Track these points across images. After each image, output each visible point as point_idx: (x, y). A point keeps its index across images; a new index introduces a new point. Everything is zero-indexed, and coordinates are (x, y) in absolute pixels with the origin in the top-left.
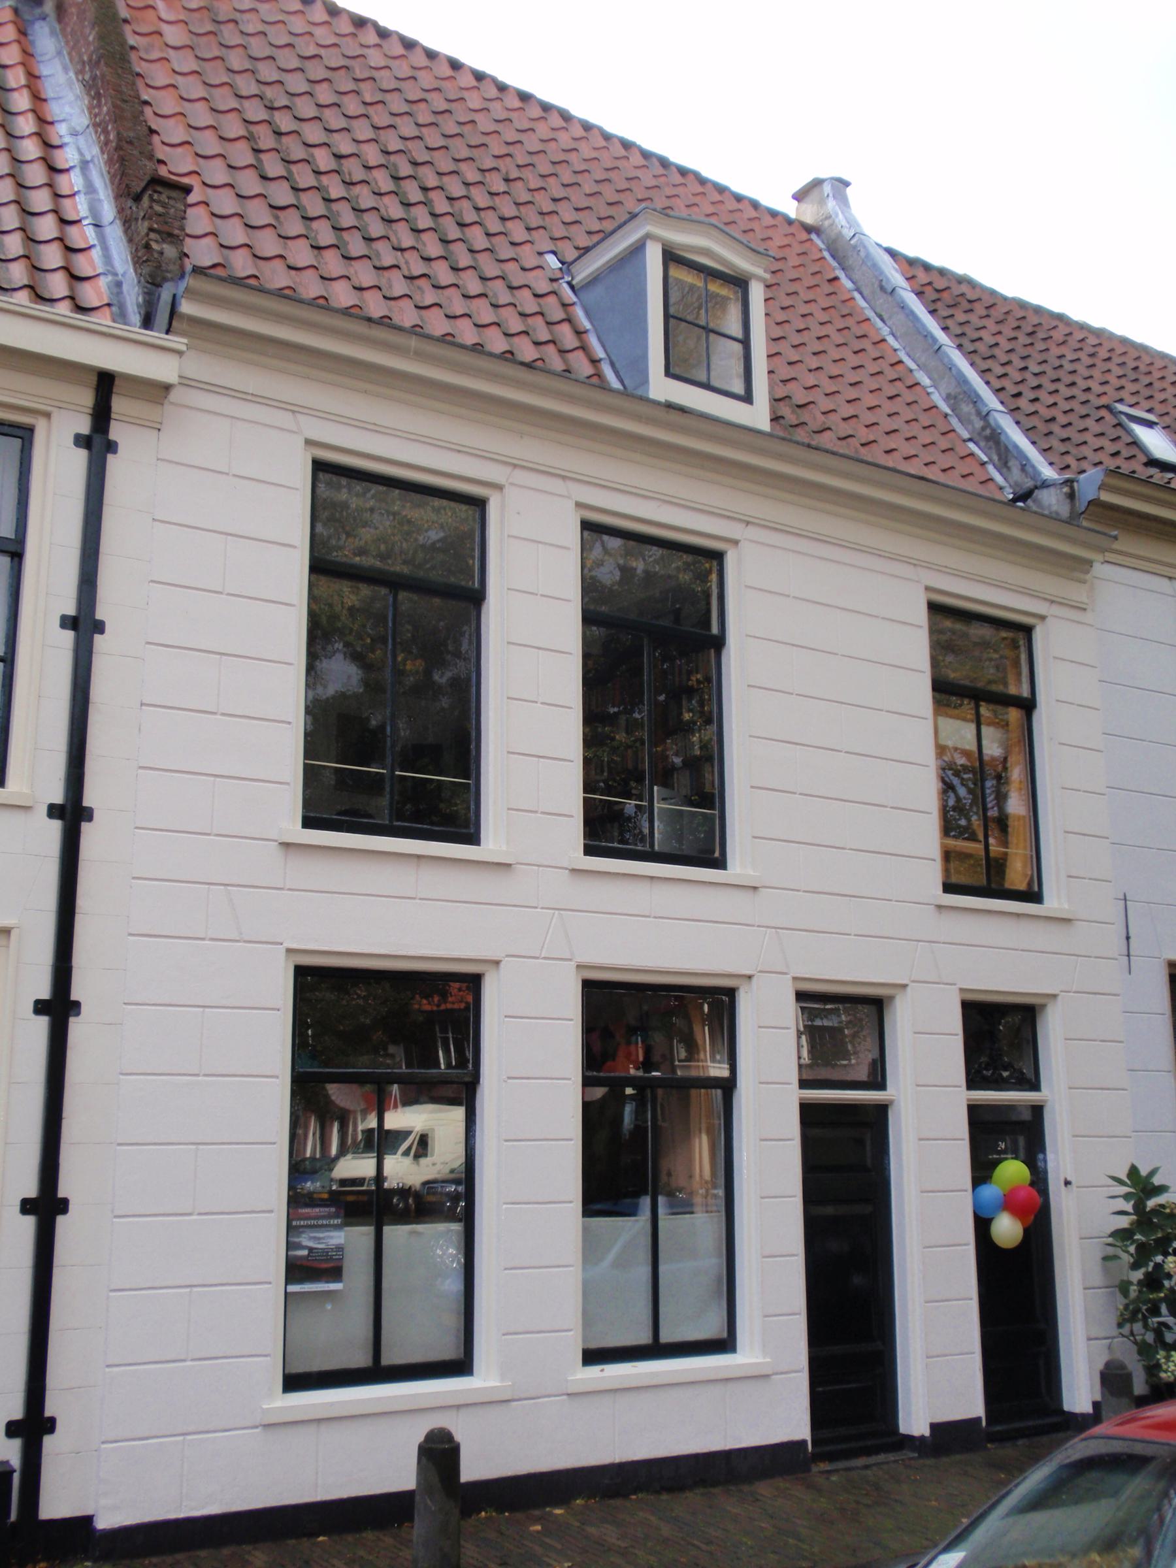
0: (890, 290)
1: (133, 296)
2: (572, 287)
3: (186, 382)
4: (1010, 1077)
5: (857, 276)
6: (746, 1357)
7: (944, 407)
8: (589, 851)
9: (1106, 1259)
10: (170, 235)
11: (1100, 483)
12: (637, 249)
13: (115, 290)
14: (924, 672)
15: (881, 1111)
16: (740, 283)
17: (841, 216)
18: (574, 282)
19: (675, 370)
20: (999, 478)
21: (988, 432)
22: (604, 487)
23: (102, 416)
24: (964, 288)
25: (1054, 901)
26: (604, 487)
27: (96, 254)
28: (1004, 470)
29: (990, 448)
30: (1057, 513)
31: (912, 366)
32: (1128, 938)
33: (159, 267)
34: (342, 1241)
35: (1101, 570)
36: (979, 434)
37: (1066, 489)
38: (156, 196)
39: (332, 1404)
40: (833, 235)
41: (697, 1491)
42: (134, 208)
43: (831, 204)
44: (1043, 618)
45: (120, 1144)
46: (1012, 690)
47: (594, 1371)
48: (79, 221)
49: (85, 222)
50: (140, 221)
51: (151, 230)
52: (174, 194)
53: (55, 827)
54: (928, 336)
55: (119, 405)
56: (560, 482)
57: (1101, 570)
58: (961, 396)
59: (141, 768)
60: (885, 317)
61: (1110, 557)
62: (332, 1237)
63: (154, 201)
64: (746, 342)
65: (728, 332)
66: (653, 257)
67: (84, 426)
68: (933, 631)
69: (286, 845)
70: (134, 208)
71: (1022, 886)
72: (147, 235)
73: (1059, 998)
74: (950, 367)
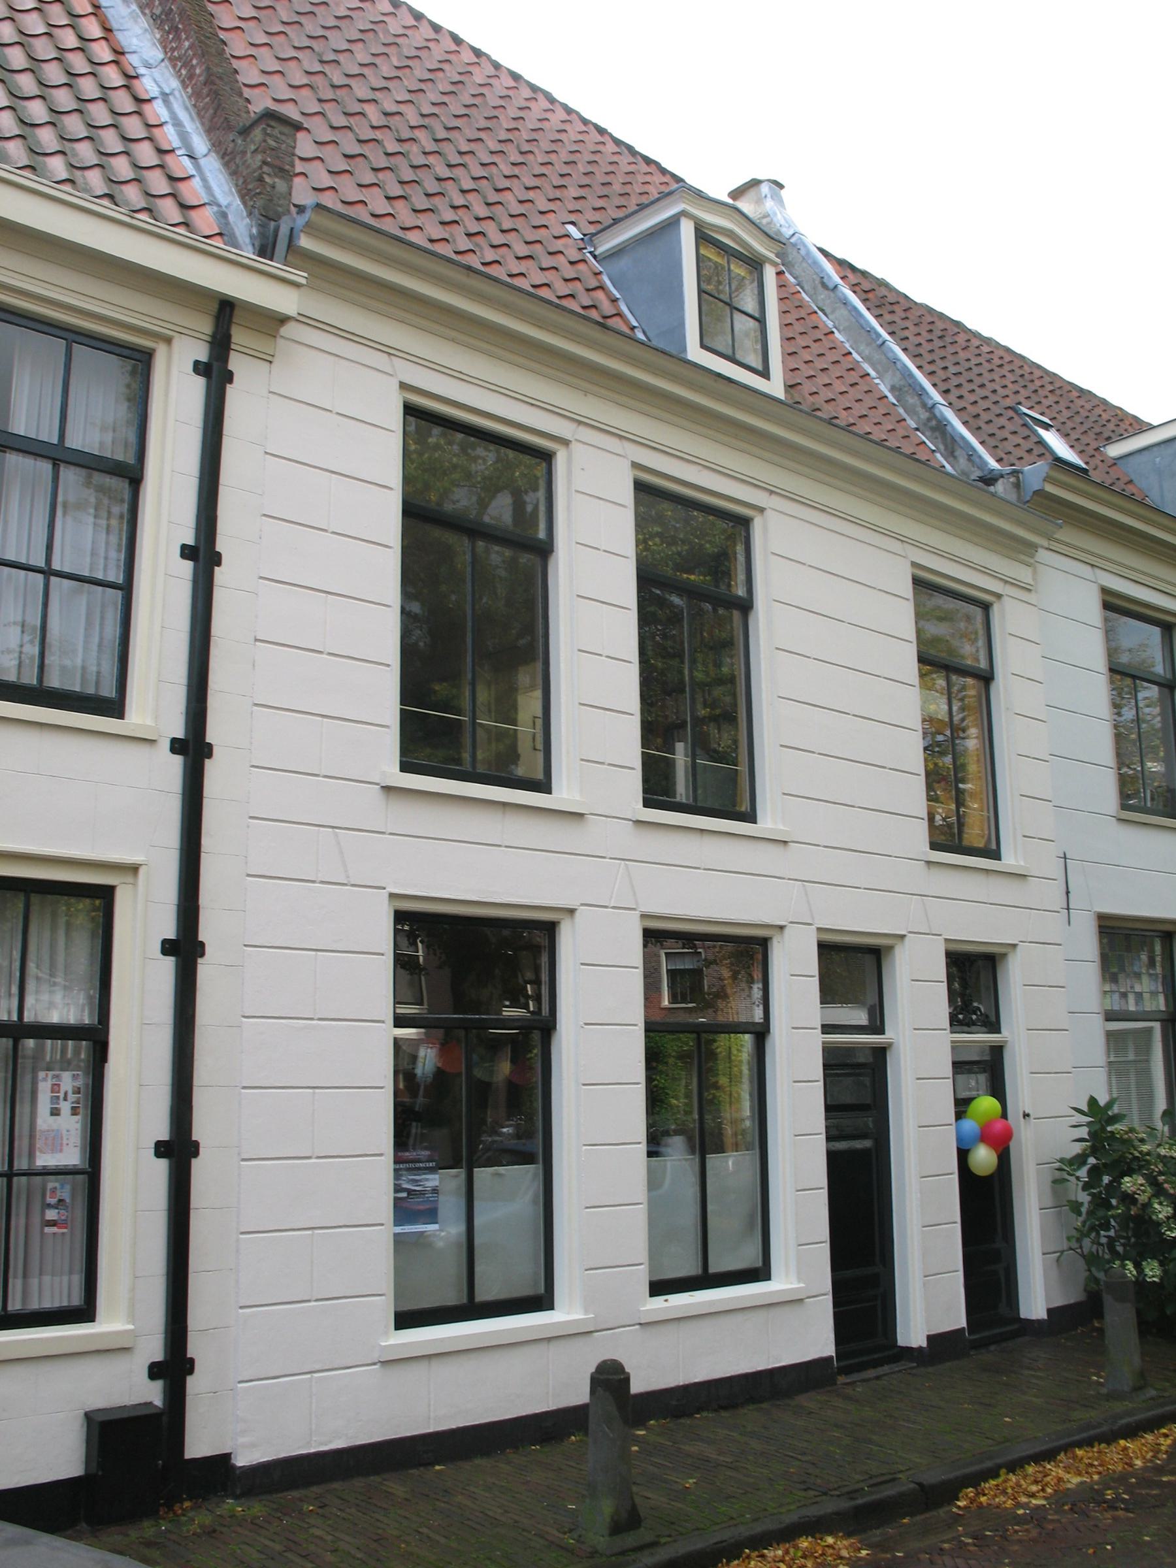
1: (243, 226)
2: (595, 257)
3: (303, 320)
4: (978, 1019)
6: (780, 1283)
7: (892, 399)
8: (647, 804)
9: (1055, 1182)
10: (282, 170)
11: (1045, 475)
12: (669, 225)
13: (223, 221)
14: (911, 642)
15: (881, 1053)
16: (755, 264)
17: (779, 216)
18: (597, 253)
19: (707, 342)
21: (934, 423)
22: (654, 448)
23: (221, 345)
24: (883, 291)
25: (1010, 859)
26: (654, 448)
27: (196, 182)
28: (951, 459)
29: (936, 438)
31: (859, 358)
32: (1068, 893)
33: (271, 200)
34: (437, 1183)
36: (925, 425)
37: (1012, 479)
38: (269, 130)
39: (442, 1340)
41: (751, 1408)
42: (239, 141)
45: (244, 1088)
47: (659, 1302)
48: (173, 151)
49: (179, 152)
50: (249, 155)
51: (265, 163)
52: (286, 130)
53: (176, 764)
54: (871, 331)
55: (239, 336)
56: (615, 441)
57: (1043, 555)
58: (906, 389)
59: (256, 705)
60: (828, 311)
61: (1055, 546)
62: (427, 1180)
63: (268, 135)
64: (761, 320)
65: (745, 309)
66: (687, 231)
67: (201, 353)
69: (388, 789)
70: (239, 141)
71: (980, 844)
72: (261, 168)
74: (895, 361)
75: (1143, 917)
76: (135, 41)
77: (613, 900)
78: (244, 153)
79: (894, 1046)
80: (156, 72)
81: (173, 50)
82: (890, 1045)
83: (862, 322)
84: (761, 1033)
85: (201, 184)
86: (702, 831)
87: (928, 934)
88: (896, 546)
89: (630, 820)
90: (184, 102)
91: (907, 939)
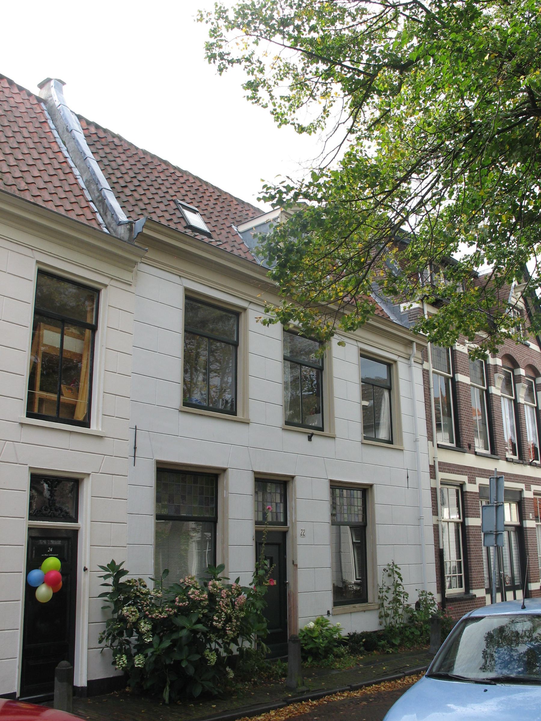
0: (70, 131)
5: (58, 123)
7: (83, 185)
20: (100, 220)
24: (116, 141)
25: (95, 427)
28: (104, 217)
30: (123, 238)
32: (135, 448)
35: (142, 267)
36: (97, 199)
40: (51, 105)
43: (53, 91)
44: (106, 286)
46: (89, 321)
54: (83, 153)
60: (66, 143)
61: (144, 260)
68: (39, 286)
73: (91, 476)
74: (89, 168)
75: (184, 464)
83: (79, 148)
87: (17, 463)
88: (28, 252)
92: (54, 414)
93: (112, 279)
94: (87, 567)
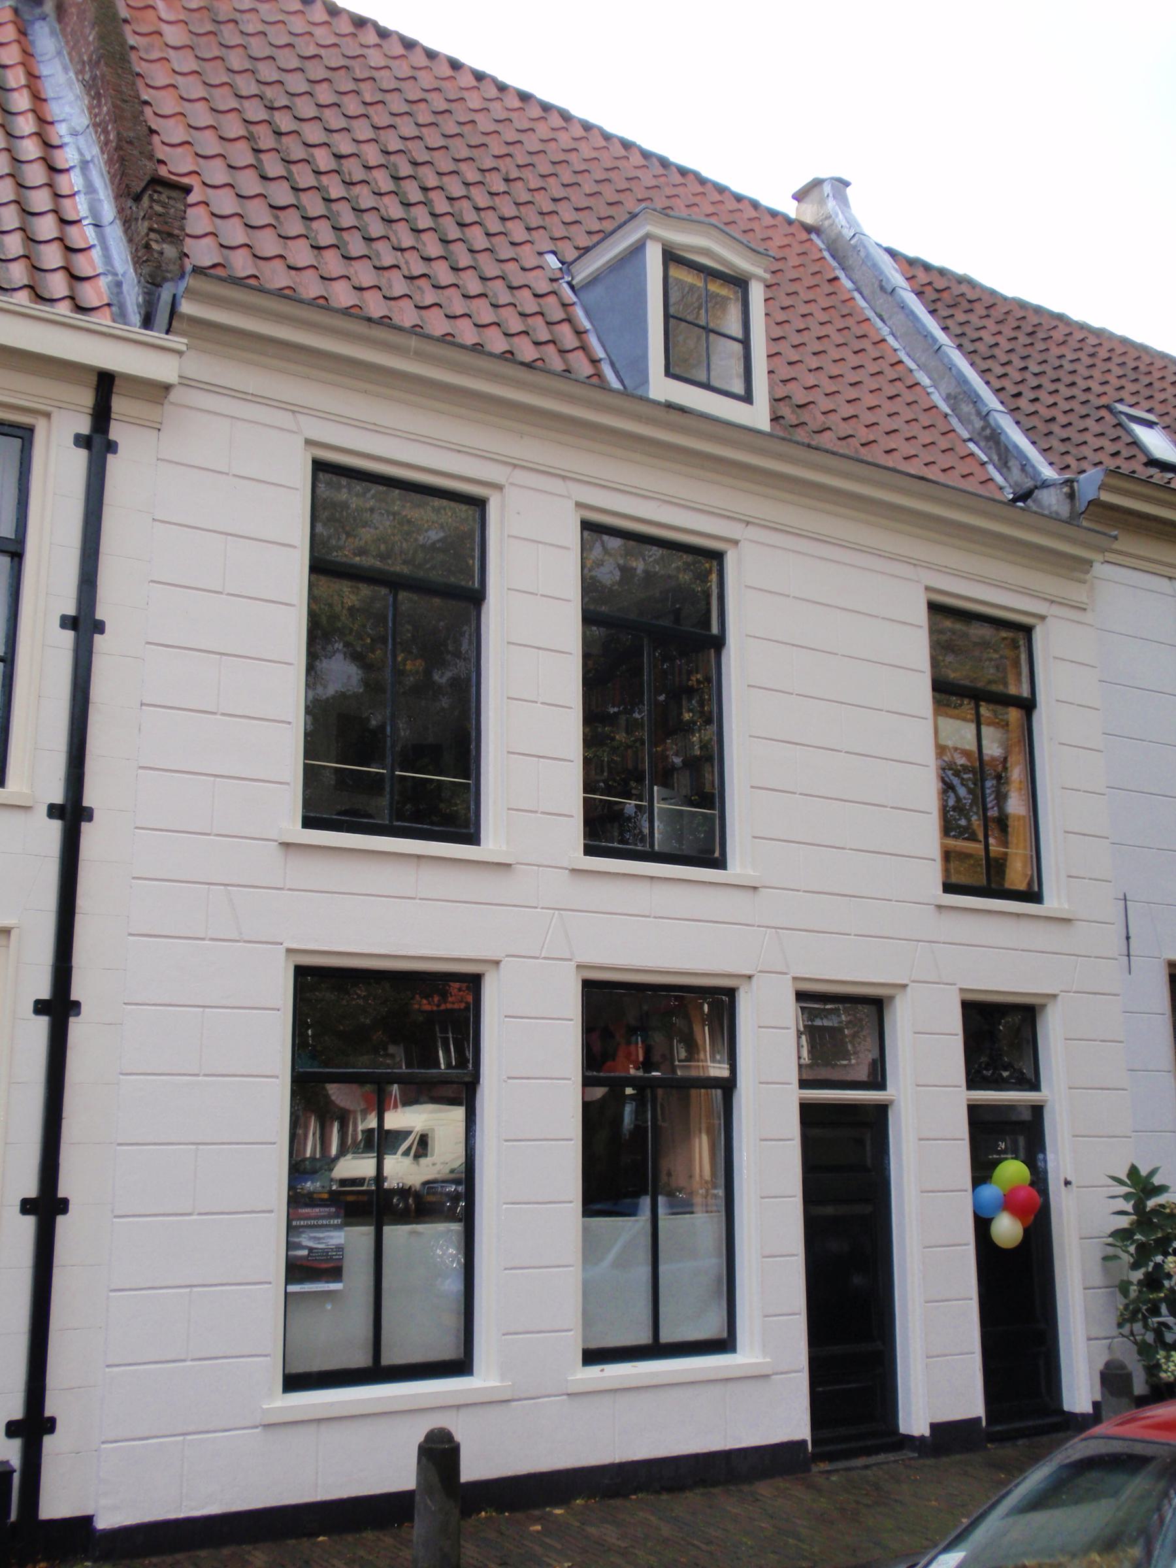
0: (890, 290)
1: (133, 296)
2: (572, 287)
3: (186, 382)
4: (1010, 1077)
5: (857, 276)
7: (944, 407)
10: (170, 235)
11: (1100, 483)
12: (637, 249)
13: (115, 290)
14: (924, 672)
15: (881, 1111)
16: (740, 283)
17: (841, 216)
18: (574, 282)
19: (675, 370)
20: (999, 478)
21: (988, 432)
22: (604, 487)
23: (102, 416)
24: (964, 288)
25: (1054, 901)
26: (604, 487)
27: (96, 254)
28: (1004, 470)
29: (990, 448)
30: (1057, 513)
31: (912, 366)
32: (1128, 938)
33: (159, 267)
34: (342, 1241)
35: (1101, 570)
36: (979, 434)
37: (1066, 489)
38: (156, 196)
40: (833, 235)
42: (134, 208)
43: (831, 204)
44: (1043, 618)
45: (120, 1144)
46: (1012, 690)
48: (79, 221)
49: (85, 222)
51: (151, 230)
52: (174, 194)
53: (55, 827)
54: (928, 336)
55: (119, 405)
56: (560, 482)
57: (1101, 570)
58: (961, 396)
59: (141, 768)
60: (885, 317)
61: (1110, 557)
62: (332, 1237)
63: (154, 201)
64: (746, 342)
65: (728, 332)
66: (653, 257)
67: (84, 426)
68: (933, 631)
69: (286, 845)
70: (134, 208)
71: (1022, 886)
72: (147, 235)
73: (1059, 998)
74: (950, 367)
76: (67, 109)
77: (544, 951)
78: (137, 219)
79: (896, 1103)
80: (81, 140)
81: (96, 116)
82: (892, 1102)
84: (728, 1086)
85: (100, 253)
86: (652, 878)
89: (566, 869)
90: (101, 168)
91: (909, 989)
92: (982, 881)
93: (1052, 602)
94: (1069, 1179)
